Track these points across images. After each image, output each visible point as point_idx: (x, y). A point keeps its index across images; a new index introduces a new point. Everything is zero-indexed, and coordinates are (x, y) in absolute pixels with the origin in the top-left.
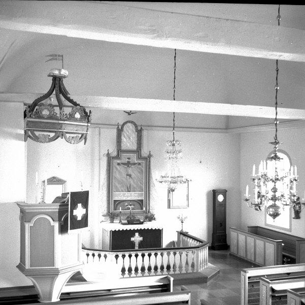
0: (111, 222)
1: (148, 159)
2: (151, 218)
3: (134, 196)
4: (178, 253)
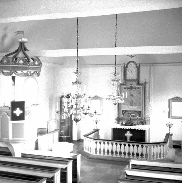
0: (118, 123)
1: (144, 85)
2: (143, 123)
3: (135, 108)
4: (144, 146)
